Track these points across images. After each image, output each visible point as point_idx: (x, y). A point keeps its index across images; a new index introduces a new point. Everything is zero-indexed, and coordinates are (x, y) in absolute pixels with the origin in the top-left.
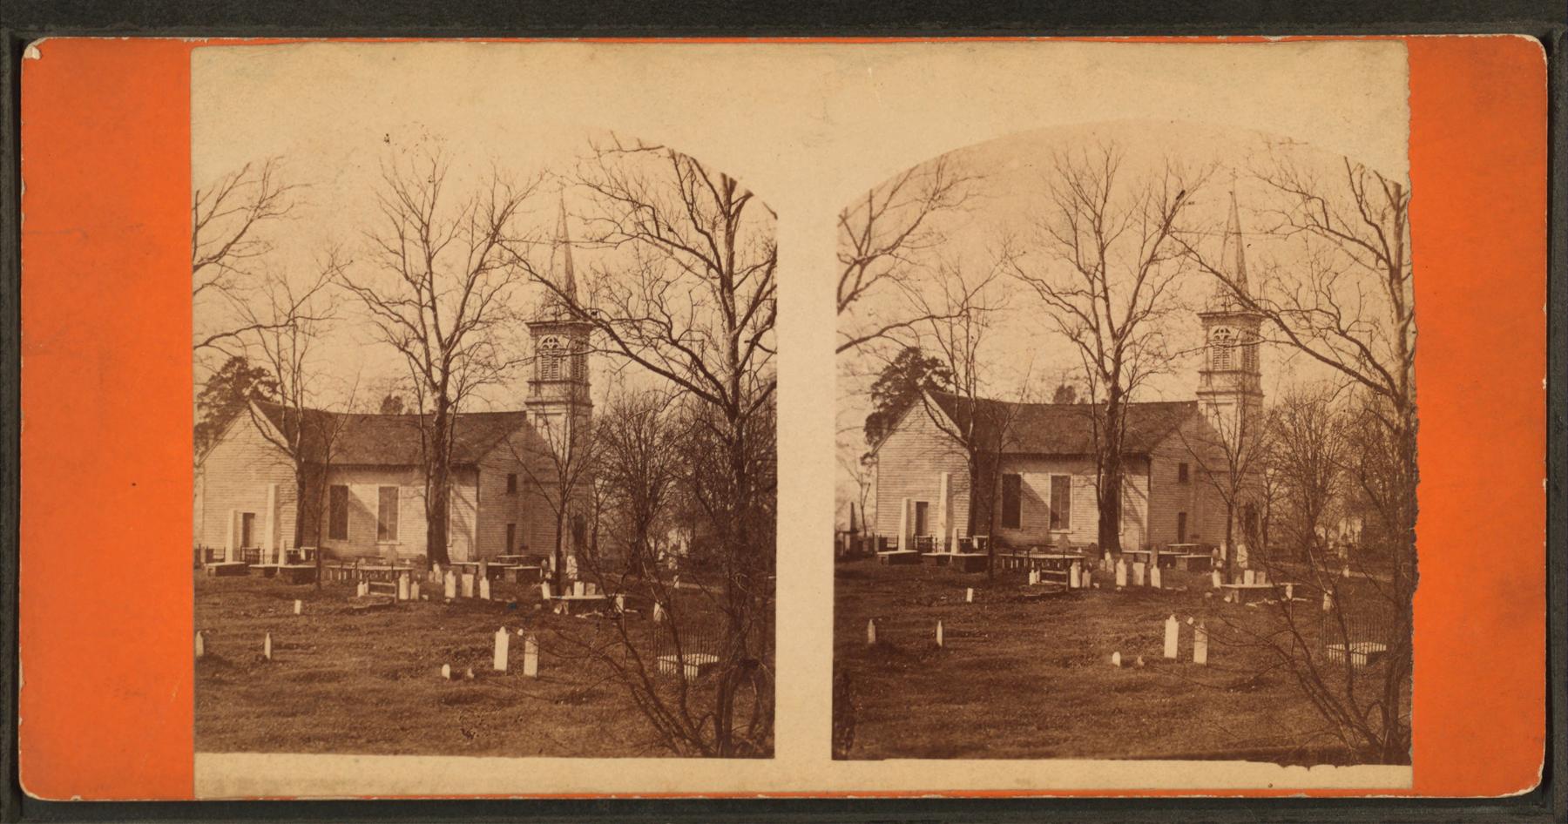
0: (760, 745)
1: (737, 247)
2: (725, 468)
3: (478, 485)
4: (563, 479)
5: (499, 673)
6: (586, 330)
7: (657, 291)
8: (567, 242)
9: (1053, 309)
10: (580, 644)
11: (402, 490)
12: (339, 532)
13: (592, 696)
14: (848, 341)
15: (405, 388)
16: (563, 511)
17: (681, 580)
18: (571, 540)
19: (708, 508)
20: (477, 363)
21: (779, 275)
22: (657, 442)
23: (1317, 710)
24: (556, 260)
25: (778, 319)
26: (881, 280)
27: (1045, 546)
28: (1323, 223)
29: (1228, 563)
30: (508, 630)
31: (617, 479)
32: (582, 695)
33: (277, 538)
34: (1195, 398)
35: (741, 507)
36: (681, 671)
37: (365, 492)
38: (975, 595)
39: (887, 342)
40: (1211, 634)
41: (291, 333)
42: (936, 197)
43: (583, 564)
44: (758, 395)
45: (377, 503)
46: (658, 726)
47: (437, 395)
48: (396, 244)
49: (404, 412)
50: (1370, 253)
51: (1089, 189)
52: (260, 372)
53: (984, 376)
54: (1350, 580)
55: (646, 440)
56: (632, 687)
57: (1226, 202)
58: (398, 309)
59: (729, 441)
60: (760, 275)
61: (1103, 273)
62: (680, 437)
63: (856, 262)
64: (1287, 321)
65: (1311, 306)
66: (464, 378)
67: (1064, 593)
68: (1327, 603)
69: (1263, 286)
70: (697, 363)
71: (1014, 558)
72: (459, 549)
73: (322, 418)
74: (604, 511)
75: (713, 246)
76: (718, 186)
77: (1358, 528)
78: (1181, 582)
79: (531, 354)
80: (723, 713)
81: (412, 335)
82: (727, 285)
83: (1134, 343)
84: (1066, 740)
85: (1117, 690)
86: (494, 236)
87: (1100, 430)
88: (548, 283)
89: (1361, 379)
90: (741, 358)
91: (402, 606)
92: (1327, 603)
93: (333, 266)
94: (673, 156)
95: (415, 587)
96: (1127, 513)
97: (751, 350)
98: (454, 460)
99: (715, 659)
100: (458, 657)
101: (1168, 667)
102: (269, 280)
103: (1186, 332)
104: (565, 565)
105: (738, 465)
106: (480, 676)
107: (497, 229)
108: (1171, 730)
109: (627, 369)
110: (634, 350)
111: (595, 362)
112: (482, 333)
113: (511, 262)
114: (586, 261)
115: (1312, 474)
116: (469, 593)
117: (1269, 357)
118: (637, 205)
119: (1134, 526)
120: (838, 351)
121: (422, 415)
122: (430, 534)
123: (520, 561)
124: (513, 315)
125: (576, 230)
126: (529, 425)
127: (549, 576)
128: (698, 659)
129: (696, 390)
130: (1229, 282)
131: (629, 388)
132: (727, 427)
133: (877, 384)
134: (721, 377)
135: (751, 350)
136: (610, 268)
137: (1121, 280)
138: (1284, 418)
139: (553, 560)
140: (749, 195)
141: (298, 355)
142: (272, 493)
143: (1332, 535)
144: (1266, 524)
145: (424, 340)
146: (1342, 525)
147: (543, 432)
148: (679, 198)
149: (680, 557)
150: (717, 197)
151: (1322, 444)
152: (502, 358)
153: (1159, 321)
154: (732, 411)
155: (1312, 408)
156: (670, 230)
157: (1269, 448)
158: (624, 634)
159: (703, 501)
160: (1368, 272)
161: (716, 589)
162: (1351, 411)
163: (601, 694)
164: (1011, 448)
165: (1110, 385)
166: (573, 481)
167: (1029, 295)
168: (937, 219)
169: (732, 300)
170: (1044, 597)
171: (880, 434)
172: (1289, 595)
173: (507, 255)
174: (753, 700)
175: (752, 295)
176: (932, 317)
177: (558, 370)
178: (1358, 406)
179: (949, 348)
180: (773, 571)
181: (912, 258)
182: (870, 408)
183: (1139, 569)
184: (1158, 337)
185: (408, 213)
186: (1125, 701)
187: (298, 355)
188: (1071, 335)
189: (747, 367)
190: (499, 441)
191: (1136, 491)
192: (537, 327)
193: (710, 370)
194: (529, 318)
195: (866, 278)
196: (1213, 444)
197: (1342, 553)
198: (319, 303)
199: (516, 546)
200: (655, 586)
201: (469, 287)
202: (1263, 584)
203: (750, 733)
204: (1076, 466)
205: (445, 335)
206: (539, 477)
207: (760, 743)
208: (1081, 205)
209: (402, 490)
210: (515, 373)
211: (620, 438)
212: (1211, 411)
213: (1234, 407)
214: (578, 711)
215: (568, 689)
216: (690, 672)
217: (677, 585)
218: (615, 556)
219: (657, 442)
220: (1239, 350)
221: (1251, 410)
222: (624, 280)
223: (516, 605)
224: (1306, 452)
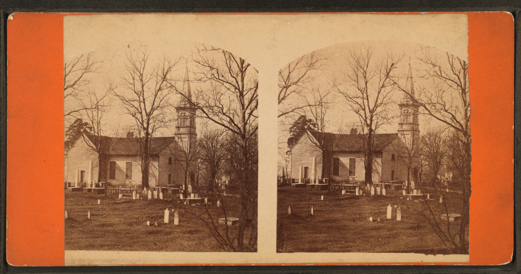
0: (252, 248)
1: (245, 82)
2: (241, 156)
3: (382, 158)
4: (187, 160)
5: (166, 224)
6: (195, 110)
7: (218, 97)
8: (188, 81)
9: (350, 103)
10: (193, 214)
11: (134, 163)
12: (113, 177)
13: (197, 231)
14: (282, 113)
15: (134, 129)
16: (187, 170)
17: (226, 193)
18: (190, 180)
19: (235, 169)
20: (158, 121)
21: (259, 91)
22: (218, 147)
23: (438, 236)
24: (185, 86)
25: (258, 106)
26: (293, 93)
27: (347, 182)
28: (439, 74)
29: (408, 187)
30: (169, 209)
31: (205, 159)
32: (193, 231)
33: (92, 179)
34: (397, 132)
35: (246, 169)
36: (226, 223)
37: (121, 164)
38: (324, 198)
39: (295, 114)
40: (402, 211)
41: (97, 111)
42: (311, 66)
43: (194, 188)
44: (252, 131)
45: (125, 167)
46: (219, 242)
47: (145, 131)
48: (132, 81)
49: (134, 137)
50: (455, 84)
51: (362, 63)
52: (86, 124)
53: (327, 125)
54: (449, 193)
55: (215, 146)
56: (210, 228)
57: (407, 67)
58: (132, 103)
59: (242, 147)
60: (252, 92)
61: (367, 91)
62: (226, 145)
63: (285, 87)
64: (428, 107)
65: (436, 102)
66: (154, 126)
67: (354, 197)
68: (441, 201)
69: (419, 95)
70: (232, 121)
71: (337, 186)
72: (152, 183)
73: (107, 139)
74: (201, 170)
75: (237, 82)
76: (239, 62)
77: (451, 176)
78: (392, 194)
79: (176, 118)
80: (240, 237)
81: (137, 111)
82: (242, 95)
83: (377, 114)
84: (354, 246)
85: (371, 229)
86: (164, 78)
87: (366, 143)
88: (182, 94)
89: (452, 126)
90: (246, 119)
91: (134, 202)
92: (441, 201)
93: (111, 89)
94: (224, 52)
95: (138, 195)
96: (374, 171)
97: (249, 116)
98: (151, 153)
99: (238, 219)
100: (152, 219)
101: (388, 222)
102: (89, 93)
103: (394, 110)
104: (188, 188)
105: (245, 155)
106: (160, 225)
107: (165, 76)
108: (389, 243)
109: (208, 123)
110: (211, 116)
111: (198, 121)
112: (160, 111)
113: (170, 87)
114: (195, 87)
115: (436, 158)
116: (156, 197)
117: (421, 119)
118: (212, 68)
119: (377, 175)
120: (279, 117)
121: (140, 138)
122: (143, 178)
123: (173, 186)
124: (171, 105)
125: (191, 77)
126: (176, 141)
127: (182, 191)
128: (232, 219)
129: (231, 130)
130: (408, 94)
131: (209, 129)
132: (242, 142)
133: (291, 128)
134: (239, 126)
135: (249, 116)
136: (203, 89)
137: (149, 95)
138: (427, 139)
139: (184, 186)
140: (249, 65)
141: (99, 118)
142: (90, 164)
143: (443, 178)
144: (420, 174)
145: (364, 110)
146: (446, 175)
147: (180, 144)
148: (226, 66)
149: (226, 185)
150: (238, 65)
151: (439, 148)
152: (167, 119)
153: (385, 107)
154: (243, 137)
155: (436, 136)
156: (223, 76)
157: (421, 149)
158: (207, 211)
159: (234, 167)
160: (454, 90)
161: (238, 196)
162: (449, 137)
163: (200, 231)
164: (336, 149)
165: (369, 128)
166: (190, 160)
167: (342, 98)
168: (311, 73)
169: (243, 100)
170: (347, 199)
171: (292, 144)
172: (428, 198)
173: (169, 85)
174: (250, 233)
175: (250, 98)
176: (310, 105)
177: (185, 123)
178: (451, 135)
179: (315, 116)
180: (257, 190)
181: (303, 86)
182: (289, 136)
183: (378, 189)
184: (385, 112)
185: (136, 71)
186: (374, 233)
187: (99, 118)
188: (356, 111)
189: (248, 122)
190: (166, 147)
191: (378, 163)
192: (178, 109)
193: (236, 123)
194: (176, 106)
195: (288, 92)
196: (403, 148)
197: (446, 184)
198: (329, 97)
199: (172, 182)
200: (218, 195)
201: (156, 95)
202: (420, 194)
203: (249, 244)
204: (357, 155)
205: (148, 111)
206: (179, 159)
207: (253, 247)
208: (359, 68)
209: (134, 163)
210: (171, 124)
211: (206, 146)
212: (402, 137)
213: (410, 136)
214: (192, 236)
215: (189, 229)
216: (229, 223)
217: (225, 195)
218: (204, 185)
219: (218, 147)
220: (412, 116)
221: (416, 136)
222: (207, 93)
223: (171, 201)
224: (434, 150)
